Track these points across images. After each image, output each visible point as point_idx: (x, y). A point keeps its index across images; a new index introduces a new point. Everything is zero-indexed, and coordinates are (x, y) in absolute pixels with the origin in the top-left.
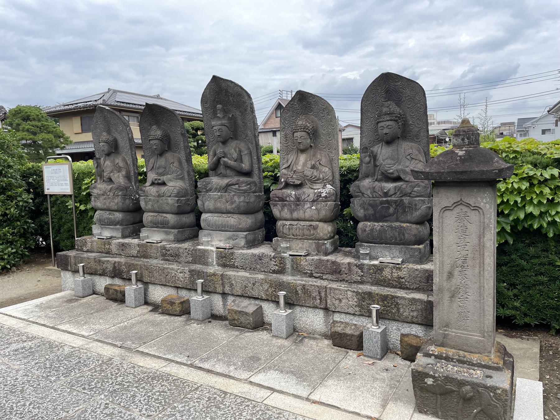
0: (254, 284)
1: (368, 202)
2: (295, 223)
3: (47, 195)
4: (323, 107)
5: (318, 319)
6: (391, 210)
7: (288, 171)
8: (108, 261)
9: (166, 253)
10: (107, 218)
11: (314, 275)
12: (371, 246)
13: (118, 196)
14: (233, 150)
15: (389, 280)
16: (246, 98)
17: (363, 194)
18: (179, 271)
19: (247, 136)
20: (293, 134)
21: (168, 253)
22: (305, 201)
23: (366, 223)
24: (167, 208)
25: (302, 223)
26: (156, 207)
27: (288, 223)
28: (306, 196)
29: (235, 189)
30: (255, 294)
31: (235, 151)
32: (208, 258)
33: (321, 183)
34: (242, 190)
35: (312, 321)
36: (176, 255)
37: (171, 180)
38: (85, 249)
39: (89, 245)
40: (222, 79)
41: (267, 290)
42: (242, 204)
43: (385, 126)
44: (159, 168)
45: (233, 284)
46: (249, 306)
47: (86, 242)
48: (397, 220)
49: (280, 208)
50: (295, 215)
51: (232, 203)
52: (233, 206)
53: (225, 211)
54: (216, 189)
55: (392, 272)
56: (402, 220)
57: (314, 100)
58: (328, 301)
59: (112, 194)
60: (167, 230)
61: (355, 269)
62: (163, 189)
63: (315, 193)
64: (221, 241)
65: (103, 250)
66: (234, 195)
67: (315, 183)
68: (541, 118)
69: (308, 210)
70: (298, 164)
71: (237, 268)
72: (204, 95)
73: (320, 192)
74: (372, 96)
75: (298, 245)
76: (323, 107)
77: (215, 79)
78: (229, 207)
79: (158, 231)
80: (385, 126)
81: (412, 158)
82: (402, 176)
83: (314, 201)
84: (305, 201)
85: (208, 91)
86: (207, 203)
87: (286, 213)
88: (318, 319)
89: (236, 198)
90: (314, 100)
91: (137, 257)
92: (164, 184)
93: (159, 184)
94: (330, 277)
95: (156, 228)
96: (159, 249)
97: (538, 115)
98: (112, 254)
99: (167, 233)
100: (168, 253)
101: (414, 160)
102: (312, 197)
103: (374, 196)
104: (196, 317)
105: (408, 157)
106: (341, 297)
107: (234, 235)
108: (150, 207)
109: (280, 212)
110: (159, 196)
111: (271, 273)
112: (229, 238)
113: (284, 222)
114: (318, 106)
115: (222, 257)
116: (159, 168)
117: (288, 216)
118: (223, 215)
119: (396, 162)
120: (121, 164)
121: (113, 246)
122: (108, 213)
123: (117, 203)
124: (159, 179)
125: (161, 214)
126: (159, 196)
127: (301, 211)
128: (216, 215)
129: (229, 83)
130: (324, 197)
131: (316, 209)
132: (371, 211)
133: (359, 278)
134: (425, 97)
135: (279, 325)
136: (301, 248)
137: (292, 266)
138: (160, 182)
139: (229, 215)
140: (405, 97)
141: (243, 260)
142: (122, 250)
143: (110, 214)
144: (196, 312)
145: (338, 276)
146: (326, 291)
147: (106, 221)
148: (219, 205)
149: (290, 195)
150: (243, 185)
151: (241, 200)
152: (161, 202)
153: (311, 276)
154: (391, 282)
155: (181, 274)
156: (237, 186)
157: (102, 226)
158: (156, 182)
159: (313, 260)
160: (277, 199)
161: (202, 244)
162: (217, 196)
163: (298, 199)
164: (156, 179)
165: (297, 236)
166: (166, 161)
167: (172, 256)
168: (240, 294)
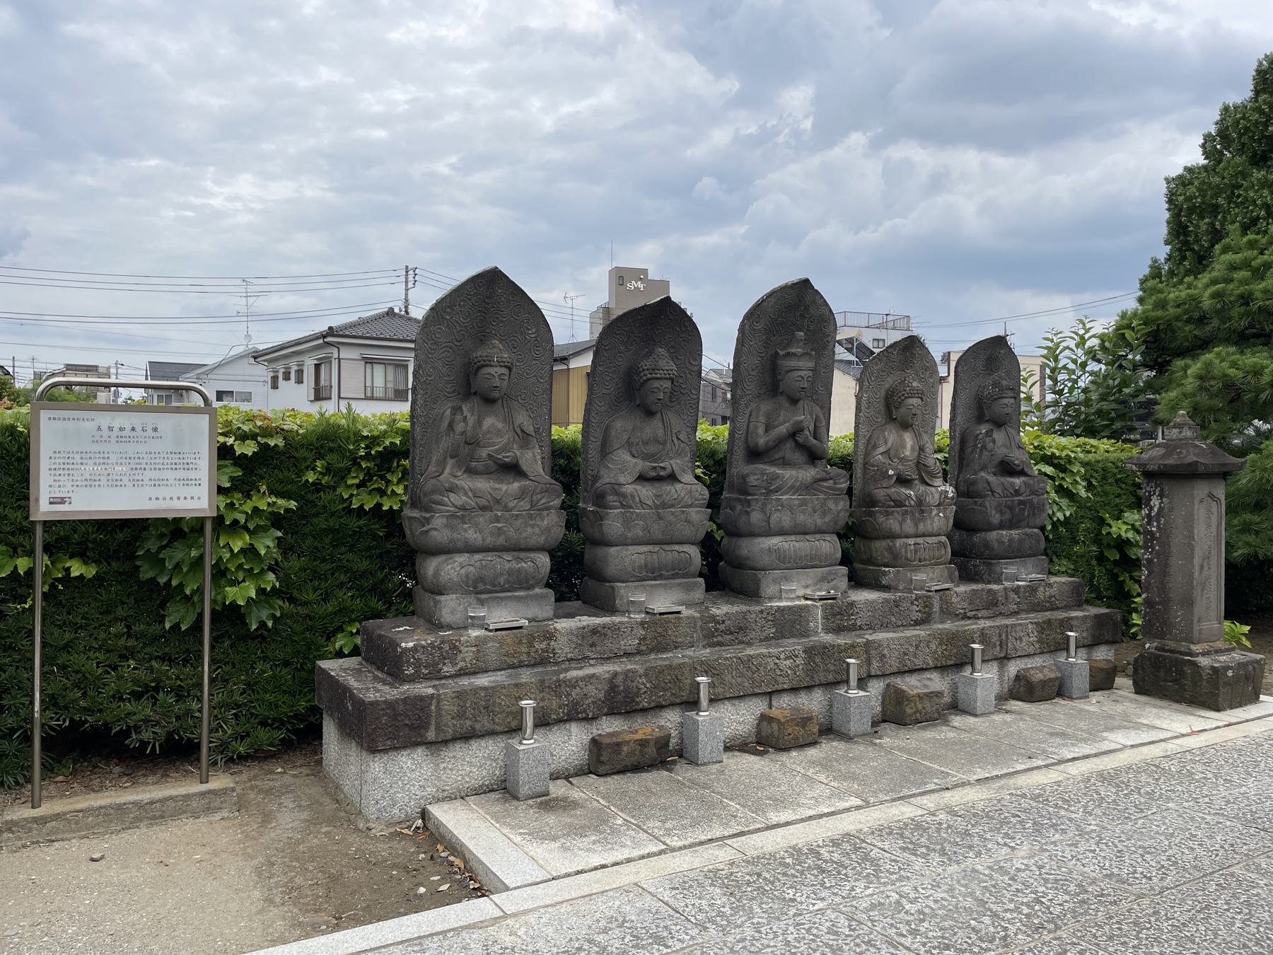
0: (917, 647)
2: (920, 540)
3: (34, 522)
8: (593, 676)
9: (717, 630)
10: (510, 573)
17: (993, 492)
18: (782, 656)
21: (722, 627)
25: (929, 540)
26: (657, 531)
27: (911, 541)
29: (828, 488)
30: (919, 663)
32: (808, 622)
36: (741, 628)
38: (448, 669)
39: (468, 654)
41: (936, 652)
42: (842, 514)
45: (884, 656)
46: (814, 702)
47: (455, 647)
49: (900, 518)
50: (921, 527)
51: (824, 514)
52: (827, 519)
53: (812, 529)
54: (792, 487)
59: (525, 504)
61: (1013, 595)
64: (806, 587)
65: (524, 657)
68: (220, 365)
69: (936, 519)
72: (758, 306)
77: (804, 286)
85: (773, 300)
86: (775, 517)
87: (909, 527)
89: (831, 505)
91: (639, 653)
96: (699, 624)
97: (211, 361)
98: (556, 663)
99: (688, 588)
100: (722, 627)
104: (861, 730)
107: (830, 573)
108: (640, 533)
110: (664, 505)
112: (823, 579)
113: (905, 540)
115: (834, 615)
118: (808, 537)
121: (563, 640)
122: (507, 556)
125: (667, 547)
128: (793, 538)
129: (818, 298)
132: (1008, 516)
137: (941, 608)
142: (593, 645)
143: (519, 559)
144: (858, 722)
147: (502, 580)
148: (801, 518)
149: (909, 497)
153: (965, 617)
155: (788, 662)
157: (483, 596)
161: (771, 599)
163: (920, 502)
167: (731, 633)
168: (895, 670)
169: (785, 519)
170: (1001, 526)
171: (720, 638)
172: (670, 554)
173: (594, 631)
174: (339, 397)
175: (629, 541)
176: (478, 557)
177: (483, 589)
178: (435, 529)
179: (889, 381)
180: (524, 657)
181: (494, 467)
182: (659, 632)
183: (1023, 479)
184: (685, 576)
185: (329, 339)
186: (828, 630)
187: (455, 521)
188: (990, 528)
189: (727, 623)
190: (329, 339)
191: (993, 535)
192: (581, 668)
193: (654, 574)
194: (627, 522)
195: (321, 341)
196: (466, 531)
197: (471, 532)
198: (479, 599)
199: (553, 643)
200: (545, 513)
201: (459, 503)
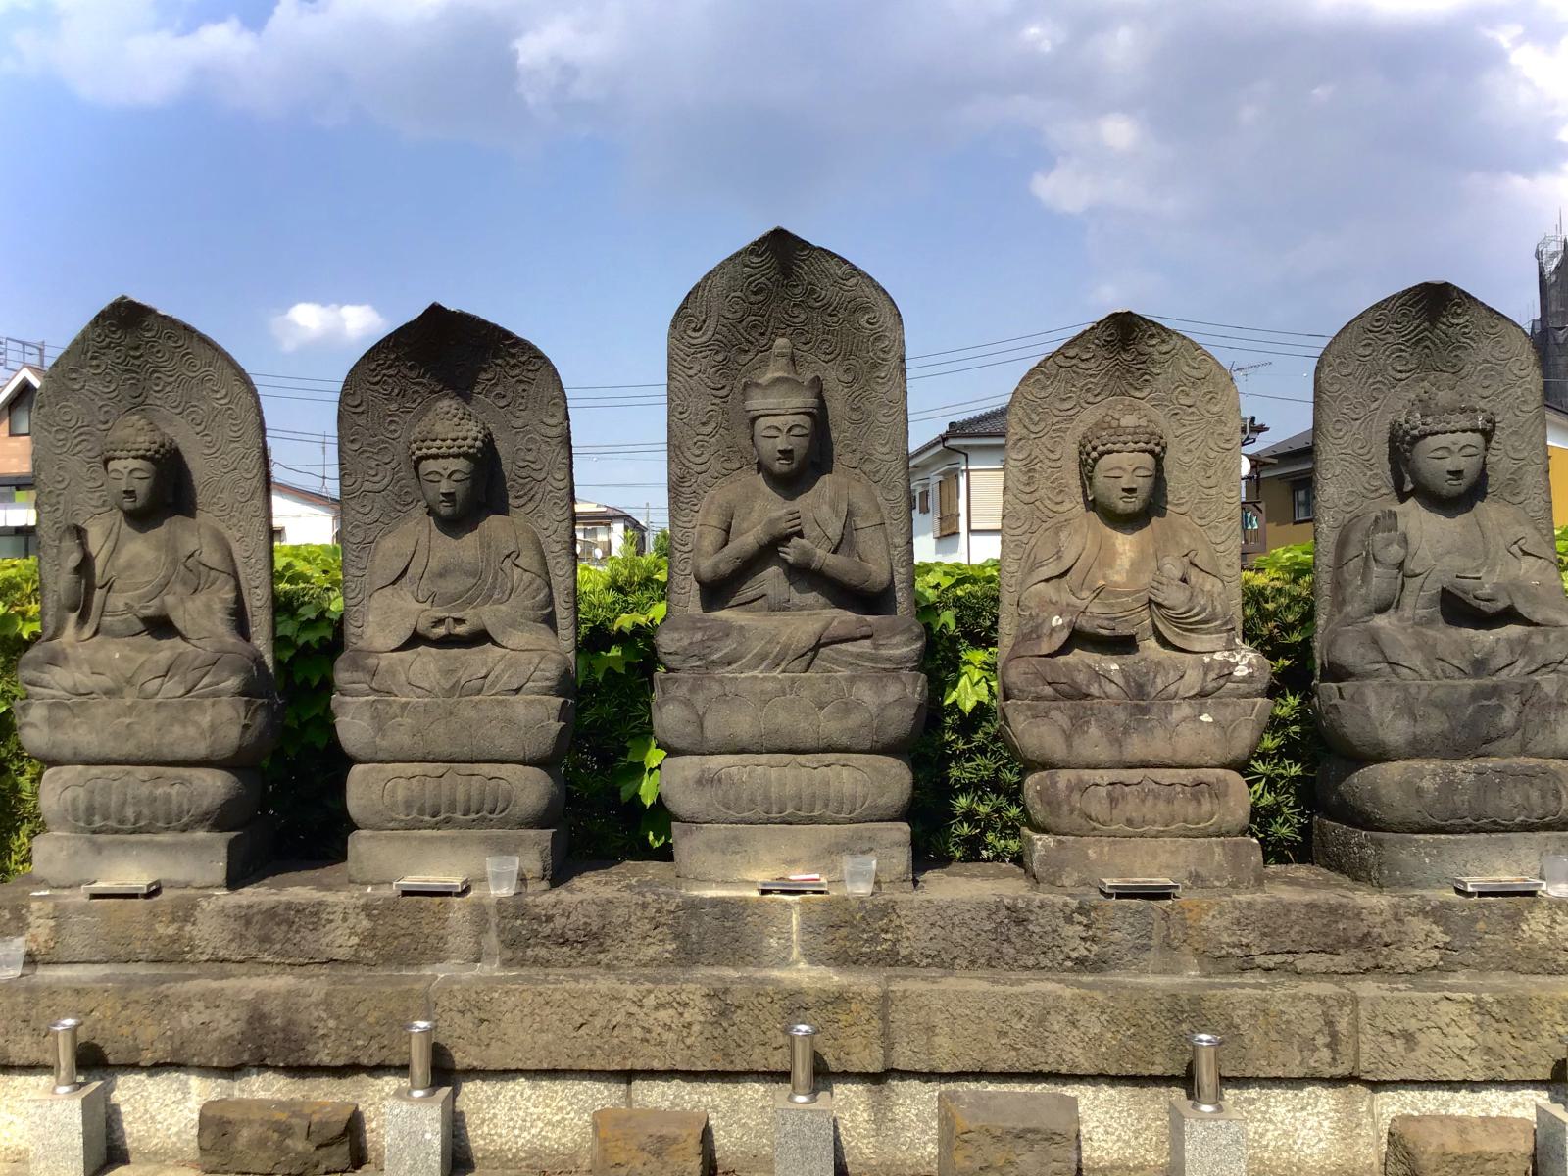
1: (1424, 693)
4: (1194, 373)
5: (1313, 1122)
6: (1508, 718)
7: (1059, 590)
9: (536, 933)
11: (1260, 960)
12: (1443, 842)
13: (217, 694)
14: (826, 508)
15: (1545, 948)
16: (890, 322)
18: (650, 1001)
19: (866, 459)
20: (416, 468)
21: (546, 929)
22: (1169, 699)
23: (1415, 763)
24: (506, 744)
26: (440, 739)
28: (1173, 675)
29: (858, 655)
31: (835, 511)
33: (1218, 631)
34: (889, 659)
35: (1286, 1133)
37: (513, 625)
40: (805, 245)
42: (894, 712)
43: (1455, 448)
44: (442, 574)
48: (1523, 751)
50: (1136, 747)
52: (855, 720)
55: (1554, 921)
56: (1538, 749)
57: (1165, 348)
58: (1365, 1048)
60: (496, 832)
62: (477, 660)
63: (1207, 668)
66: (852, 680)
67: (1191, 631)
69: (1184, 728)
70: (1111, 566)
71: (911, 963)
73: (1227, 664)
74: (1361, 351)
75: (1155, 855)
76: (1194, 373)
78: (831, 726)
79: (453, 839)
80: (1455, 448)
81: (1525, 553)
82: (1523, 609)
83: (1203, 694)
84: (1169, 699)
88: (1313, 1122)
90: (1165, 348)
92: (480, 637)
93: (448, 642)
94: (1322, 962)
95: (436, 826)
101: (1531, 559)
102: (1193, 681)
103: (1438, 673)
105: (1515, 549)
106: (1412, 1025)
109: (1068, 738)
110: (456, 690)
111: (1070, 970)
113: (1088, 775)
114: (1178, 369)
116: (442, 574)
117: (1103, 752)
119: (1483, 565)
120: (211, 556)
123: (213, 728)
124: (459, 621)
126: (456, 690)
127: (1160, 733)
128: (764, 758)
130: (1243, 680)
131: (1216, 723)
133: (1435, 955)
134: (903, 371)
135: (1216, 1164)
136: (856, 876)
138: (460, 630)
139: (831, 757)
140: (1476, 364)
141: (936, 931)
145: (1355, 955)
146: (1355, 1012)
150: (894, 641)
151: (889, 698)
152: (470, 713)
154: (1550, 955)
156: (867, 642)
157: (102, 838)
158: (441, 631)
159: (1250, 905)
160: (1048, 690)
162: (769, 686)
164: (440, 622)
165: (1144, 822)
166: (486, 545)
169: (743, 724)
170: (1417, 749)
171: (542, 952)
172: (463, 783)
173: (272, 914)
174: (970, 531)
175: (381, 755)
176: (96, 770)
177: (105, 826)
178: (32, 725)
179: (1397, 406)
180: (138, 946)
181: (140, 627)
182: (408, 928)
183: (1514, 631)
184: (503, 824)
185: (951, 442)
186: (813, 958)
187: (63, 714)
188: (1382, 756)
189: (559, 922)
190: (951, 442)
191: (1388, 775)
192: (1020, 982)
193: (435, 817)
194: (380, 722)
195: (940, 447)
196: (75, 728)
197: (82, 731)
198: (94, 843)
199: (189, 928)
200: (208, 702)
201: (68, 683)
